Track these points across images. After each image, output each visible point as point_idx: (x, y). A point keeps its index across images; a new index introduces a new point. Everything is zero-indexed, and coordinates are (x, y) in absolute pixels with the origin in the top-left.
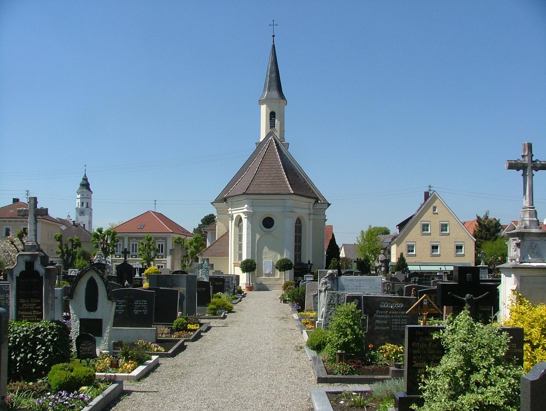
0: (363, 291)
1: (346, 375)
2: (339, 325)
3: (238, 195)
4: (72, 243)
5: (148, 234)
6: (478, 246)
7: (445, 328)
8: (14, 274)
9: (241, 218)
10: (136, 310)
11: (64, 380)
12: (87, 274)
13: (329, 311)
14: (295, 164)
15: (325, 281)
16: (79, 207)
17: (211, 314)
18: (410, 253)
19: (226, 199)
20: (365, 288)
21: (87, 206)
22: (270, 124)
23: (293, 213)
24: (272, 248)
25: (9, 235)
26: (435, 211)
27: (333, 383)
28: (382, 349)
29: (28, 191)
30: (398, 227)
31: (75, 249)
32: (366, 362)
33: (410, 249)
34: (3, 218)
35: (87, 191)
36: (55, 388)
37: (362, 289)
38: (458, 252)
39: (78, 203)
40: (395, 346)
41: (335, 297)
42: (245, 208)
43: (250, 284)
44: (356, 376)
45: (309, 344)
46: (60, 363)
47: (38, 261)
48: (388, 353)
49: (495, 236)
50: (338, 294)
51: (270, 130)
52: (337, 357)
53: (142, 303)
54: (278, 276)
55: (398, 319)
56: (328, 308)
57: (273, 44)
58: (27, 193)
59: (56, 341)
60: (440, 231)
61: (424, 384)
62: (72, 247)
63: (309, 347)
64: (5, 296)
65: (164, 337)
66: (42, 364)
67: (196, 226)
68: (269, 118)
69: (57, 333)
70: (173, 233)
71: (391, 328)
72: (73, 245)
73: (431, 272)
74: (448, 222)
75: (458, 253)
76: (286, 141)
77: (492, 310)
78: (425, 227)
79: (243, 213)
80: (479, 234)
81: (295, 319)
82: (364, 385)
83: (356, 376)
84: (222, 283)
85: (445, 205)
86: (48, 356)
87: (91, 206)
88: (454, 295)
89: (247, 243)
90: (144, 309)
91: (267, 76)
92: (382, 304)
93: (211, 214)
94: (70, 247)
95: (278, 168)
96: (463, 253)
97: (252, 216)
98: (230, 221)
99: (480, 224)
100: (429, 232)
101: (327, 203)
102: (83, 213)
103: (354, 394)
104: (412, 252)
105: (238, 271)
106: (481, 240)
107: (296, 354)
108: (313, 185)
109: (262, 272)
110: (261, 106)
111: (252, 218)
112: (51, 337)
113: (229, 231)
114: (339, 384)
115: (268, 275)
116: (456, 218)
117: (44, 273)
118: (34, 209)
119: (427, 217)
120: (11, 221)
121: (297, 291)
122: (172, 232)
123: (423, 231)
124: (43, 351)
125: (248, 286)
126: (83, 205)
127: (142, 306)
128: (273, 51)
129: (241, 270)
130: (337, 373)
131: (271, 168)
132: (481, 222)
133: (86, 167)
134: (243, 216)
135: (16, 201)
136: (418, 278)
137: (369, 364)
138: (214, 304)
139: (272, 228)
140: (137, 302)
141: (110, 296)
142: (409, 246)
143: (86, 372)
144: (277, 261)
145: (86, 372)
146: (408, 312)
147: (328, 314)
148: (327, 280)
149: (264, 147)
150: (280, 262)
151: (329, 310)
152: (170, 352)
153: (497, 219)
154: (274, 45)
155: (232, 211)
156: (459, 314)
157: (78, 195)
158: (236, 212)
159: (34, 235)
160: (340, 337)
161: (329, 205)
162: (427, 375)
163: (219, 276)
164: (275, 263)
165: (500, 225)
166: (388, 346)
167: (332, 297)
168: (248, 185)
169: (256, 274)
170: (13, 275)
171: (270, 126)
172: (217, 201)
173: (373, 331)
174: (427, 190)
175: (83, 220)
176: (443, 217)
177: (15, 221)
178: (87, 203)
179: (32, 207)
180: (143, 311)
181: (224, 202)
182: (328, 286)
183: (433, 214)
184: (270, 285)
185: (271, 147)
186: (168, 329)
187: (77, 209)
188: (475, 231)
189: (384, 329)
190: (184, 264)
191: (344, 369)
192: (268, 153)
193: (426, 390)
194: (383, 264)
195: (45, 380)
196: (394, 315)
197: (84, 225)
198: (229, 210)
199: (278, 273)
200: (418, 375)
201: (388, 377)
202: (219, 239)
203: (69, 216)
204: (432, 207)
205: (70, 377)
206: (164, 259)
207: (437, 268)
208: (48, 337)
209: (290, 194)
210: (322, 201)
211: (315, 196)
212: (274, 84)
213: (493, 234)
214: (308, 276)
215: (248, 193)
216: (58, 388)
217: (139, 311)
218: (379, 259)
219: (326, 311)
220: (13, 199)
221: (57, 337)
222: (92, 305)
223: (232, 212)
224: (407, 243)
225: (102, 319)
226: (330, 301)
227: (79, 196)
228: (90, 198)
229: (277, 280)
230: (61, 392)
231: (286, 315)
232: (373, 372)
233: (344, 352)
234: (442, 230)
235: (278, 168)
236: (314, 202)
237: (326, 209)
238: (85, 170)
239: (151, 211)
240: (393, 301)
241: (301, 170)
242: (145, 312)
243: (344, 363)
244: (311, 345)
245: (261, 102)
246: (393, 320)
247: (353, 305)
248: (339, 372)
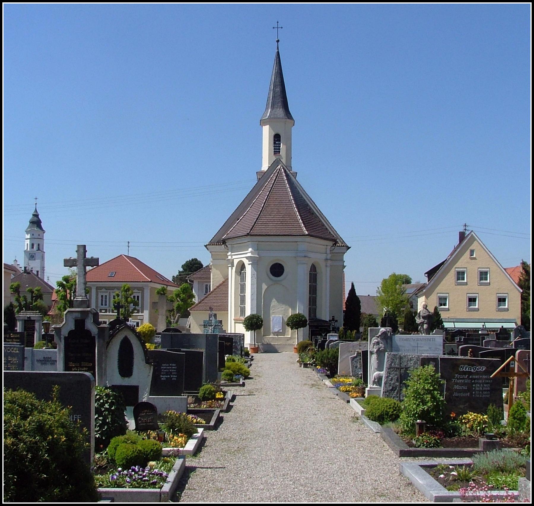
0: (421, 352)
1: (431, 447)
2: (416, 392)
4: (32, 294)
5: (125, 283)
8: (62, 333)
9: (244, 264)
10: (163, 375)
11: (132, 454)
12: (120, 333)
13: (389, 376)
14: (307, 198)
15: (377, 341)
17: (228, 380)
19: (225, 241)
21: (39, 248)
22: (274, 149)
23: (306, 259)
24: (282, 301)
26: (473, 255)
27: (418, 457)
28: (464, 418)
30: (426, 275)
31: (35, 302)
32: (448, 434)
33: (442, 301)
35: (39, 229)
37: (420, 350)
38: (501, 306)
39: (27, 244)
40: (479, 415)
41: (396, 360)
42: (249, 253)
43: (255, 344)
44: (442, 449)
45: (369, 414)
46: (119, 435)
47: (89, 318)
48: (471, 423)
52: (417, 427)
53: (171, 368)
54: (289, 335)
56: (388, 372)
57: (277, 51)
59: (114, 410)
60: (479, 280)
62: (32, 299)
63: (369, 417)
66: (99, 436)
68: (272, 142)
70: (151, 281)
71: (471, 394)
72: (32, 297)
73: (468, 330)
74: (488, 269)
75: (500, 307)
78: (460, 275)
79: (247, 258)
81: (329, 386)
82: (453, 458)
83: (442, 449)
86: (106, 427)
87: (43, 249)
89: (252, 295)
90: (172, 375)
91: (270, 90)
94: (29, 300)
95: (289, 203)
96: (506, 307)
97: (257, 262)
98: (230, 268)
100: (465, 281)
102: (33, 256)
103: (451, 467)
104: (444, 306)
105: (240, 329)
107: (355, 426)
109: (270, 330)
110: (263, 126)
112: (109, 405)
113: (228, 279)
114: (424, 457)
115: (277, 333)
116: (498, 263)
117: (97, 332)
118: (84, 259)
119: (463, 263)
122: (150, 280)
123: (481, 280)
124: (101, 422)
125: (253, 347)
126: (33, 248)
127: (170, 370)
128: (278, 59)
129: (244, 328)
133: (37, 199)
134: (246, 262)
136: (463, 337)
137: (451, 436)
138: (229, 368)
140: (164, 366)
142: (440, 299)
143: (153, 445)
145: (153, 445)
146: (493, 377)
147: (389, 380)
148: (379, 339)
149: (271, 178)
150: (292, 318)
151: (390, 374)
152: (212, 423)
154: (278, 52)
155: (232, 256)
157: (27, 235)
158: (237, 257)
159: (83, 288)
160: (418, 405)
161: (349, 248)
163: (224, 335)
164: (286, 320)
166: (471, 416)
167: (393, 360)
168: (253, 225)
169: (262, 333)
170: (61, 335)
171: (274, 152)
172: (212, 243)
175: (35, 266)
176: (482, 264)
178: (39, 245)
180: (172, 376)
181: (222, 245)
182: (380, 346)
183: (469, 259)
184: (279, 346)
185: (279, 178)
186: (192, 398)
187: (25, 251)
188: (520, 280)
189: (464, 395)
190: (169, 321)
191: (428, 441)
192: (276, 185)
194: (426, 320)
195: (104, 454)
196: (475, 379)
197: (38, 272)
198: (228, 254)
199: (289, 331)
203: (15, 260)
204: (468, 252)
205: (137, 450)
206: (140, 314)
207: (479, 325)
208: (105, 405)
212: (279, 100)
214: (331, 335)
215: (252, 234)
216: (125, 463)
217: (166, 376)
219: (386, 375)
221: (115, 406)
224: (439, 295)
226: (391, 365)
227: (28, 236)
228: (42, 239)
229: (288, 340)
230: (134, 467)
232: (457, 445)
234: (481, 279)
235: (289, 203)
237: (344, 253)
238: (36, 204)
240: (473, 363)
241: (314, 205)
242: (174, 377)
243: (426, 435)
244: (372, 415)
245: (263, 122)
247: (430, 368)
248: (422, 445)
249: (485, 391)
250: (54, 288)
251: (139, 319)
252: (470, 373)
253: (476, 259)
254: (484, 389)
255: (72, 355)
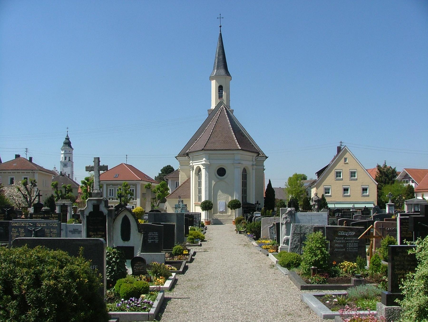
0: (313, 223)
1: (320, 284)
2: (311, 248)
3: (198, 151)
4: (66, 189)
5: (125, 181)
6: (379, 188)
7: (416, 247)
11: (130, 290)
12: (122, 213)
13: (294, 239)
15: (285, 216)
16: (63, 160)
18: (326, 194)
20: (315, 221)
21: (69, 160)
22: (219, 95)
23: (240, 165)
24: (225, 191)
25: (13, 184)
26: (346, 161)
27: (312, 290)
28: (342, 265)
29: (26, 149)
30: (316, 174)
31: (67, 194)
33: (327, 191)
34: (8, 170)
35: (69, 148)
36: (124, 296)
37: (313, 222)
39: (62, 157)
40: (351, 263)
42: (204, 161)
43: (208, 219)
44: (327, 284)
46: (122, 278)
48: (346, 268)
49: (392, 180)
50: (300, 226)
51: (219, 101)
52: (312, 271)
53: (154, 235)
55: (351, 243)
56: (293, 236)
57: (220, 33)
58: (26, 150)
60: (350, 177)
61: (403, 285)
62: (66, 192)
63: (281, 265)
64: (50, 230)
65: (168, 260)
67: (157, 175)
69: (119, 256)
70: (141, 180)
71: (346, 250)
72: (66, 191)
73: (343, 209)
74: (356, 170)
76: (231, 108)
77: (414, 237)
78: (338, 174)
79: (202, 164)
80: (379, 179)
82: (335, 291)
83: (327, 284)
84: (191, 219)
85: (354, 157)
86: (113, 273)
87: (72, 160)
88: (422, 224)
91: (216, 58)
92: (339, 233)
93: (168, 165)
94: (64, 193)
95: (229, 129)
96: (368, 194)
98: (191, 171)
99: (380, 171)
100: (341, 178)
101: (265, 156)
103: (333, 296)
104: (328, 193)
105: (199, 210)
106: (382, 184)
107: (272, 271)
108: (254, 143)
111: (209, 169)
112: (115, 259)
113: (190, 178)
115: (222, 212)
116: (362, 166)
117: (107, 213)
118: (98, 166)
119: (340, 166)
120: (15, 173)
121: (254, 224)
124: (110, 270)
125: (207, 221)
126: (66, 159)
127: (154, 236)
128: (221, 38)
129: (201, 209)
130: (314, 283)
131: (223, 129)
132: (381, 170)
134: (202, 167)
135: (17, 156)
136: (341, 213)
137: (333, 276)
138: (191, 235)
139: (224, 177)
141: (140, 230)
144: (229, 202)
146: (360, 238)
147: (293, 241)
148: (287, 215)
150: (232, 202)
152: (181, 270)
153: (393, 168)
154: (221, 33)
155: (192, 163)
156: (426, 237)
157: (62, 151)
158: (195, 164)
160: (312, 257)
161: (267, 157)
162: (405, 279)
164: (227, 203)
165: (396, 172)
166: (346, 263)
167: (296, 228)
168: (206, 143)
169: (212, 212)
170: (84, 214)
171: (219, 97)
172: (180, 155)
173: (333, 252)
174: (339, 145)
175: (67, 171)
176: (352, 166)
177: (18, 173)
178: (69, 158)
179: (97, 165)
180: (155, 240)
183: (344, 164)
186: (168, 254)
188: (376, 177)
191: (319, 280)
192: (220, 118)
193: (404, 289)
195: (112, 290)
196: (348, 240)
197: (69, 175)
198: (190, 162)
199: (229, 210)
200: (399, 279)
201: (352, 285)
202: (182, 185)
204: (343, 159)
205: (133, 288)
206: (134, 201)
207: (351, 206)
209: (239, 150)
210: (261, 154)
211: (257, 151)
212: (222, 64)
213: (390, 179)
214: (256, 213)
215: (205, 149)
216: (126, 296)
217: (152, 240)
218: (313, 199)
220: (16, 155)
222: (126, 236)
223: (192, 164)
225: (134, 247)
226: (295, 231)
227: (63, 152)
228: (72, 154)
229: (229, 216)
231: (246, 242)
232: (337, 282)
233: (316, 267)
235: (229, 129)
236: (256, 156)
237: (264, 161)
238: (67, 132)
239: (124, 164)
240: (347, 230)
241: (245, 131)
242: (157, 241)
244: (283, 264)
245: (211, 78)
246: (348, 244)
247: (320, 233)
248: (315, 282)
249: (355, 247)
250: (79, 185)
251: (134, 204)
252: (345, 236)
253: (348, 164)
254: (354, 246)
255: (91, 227)
